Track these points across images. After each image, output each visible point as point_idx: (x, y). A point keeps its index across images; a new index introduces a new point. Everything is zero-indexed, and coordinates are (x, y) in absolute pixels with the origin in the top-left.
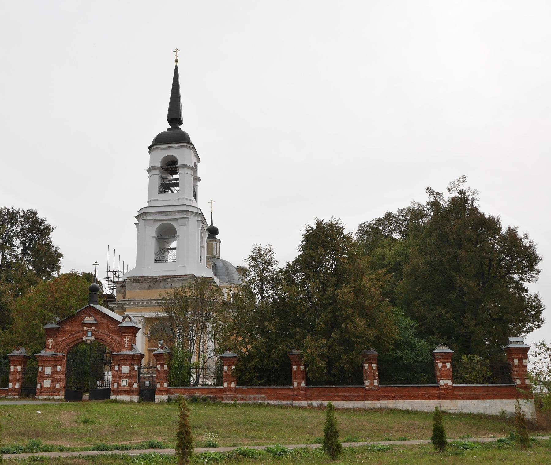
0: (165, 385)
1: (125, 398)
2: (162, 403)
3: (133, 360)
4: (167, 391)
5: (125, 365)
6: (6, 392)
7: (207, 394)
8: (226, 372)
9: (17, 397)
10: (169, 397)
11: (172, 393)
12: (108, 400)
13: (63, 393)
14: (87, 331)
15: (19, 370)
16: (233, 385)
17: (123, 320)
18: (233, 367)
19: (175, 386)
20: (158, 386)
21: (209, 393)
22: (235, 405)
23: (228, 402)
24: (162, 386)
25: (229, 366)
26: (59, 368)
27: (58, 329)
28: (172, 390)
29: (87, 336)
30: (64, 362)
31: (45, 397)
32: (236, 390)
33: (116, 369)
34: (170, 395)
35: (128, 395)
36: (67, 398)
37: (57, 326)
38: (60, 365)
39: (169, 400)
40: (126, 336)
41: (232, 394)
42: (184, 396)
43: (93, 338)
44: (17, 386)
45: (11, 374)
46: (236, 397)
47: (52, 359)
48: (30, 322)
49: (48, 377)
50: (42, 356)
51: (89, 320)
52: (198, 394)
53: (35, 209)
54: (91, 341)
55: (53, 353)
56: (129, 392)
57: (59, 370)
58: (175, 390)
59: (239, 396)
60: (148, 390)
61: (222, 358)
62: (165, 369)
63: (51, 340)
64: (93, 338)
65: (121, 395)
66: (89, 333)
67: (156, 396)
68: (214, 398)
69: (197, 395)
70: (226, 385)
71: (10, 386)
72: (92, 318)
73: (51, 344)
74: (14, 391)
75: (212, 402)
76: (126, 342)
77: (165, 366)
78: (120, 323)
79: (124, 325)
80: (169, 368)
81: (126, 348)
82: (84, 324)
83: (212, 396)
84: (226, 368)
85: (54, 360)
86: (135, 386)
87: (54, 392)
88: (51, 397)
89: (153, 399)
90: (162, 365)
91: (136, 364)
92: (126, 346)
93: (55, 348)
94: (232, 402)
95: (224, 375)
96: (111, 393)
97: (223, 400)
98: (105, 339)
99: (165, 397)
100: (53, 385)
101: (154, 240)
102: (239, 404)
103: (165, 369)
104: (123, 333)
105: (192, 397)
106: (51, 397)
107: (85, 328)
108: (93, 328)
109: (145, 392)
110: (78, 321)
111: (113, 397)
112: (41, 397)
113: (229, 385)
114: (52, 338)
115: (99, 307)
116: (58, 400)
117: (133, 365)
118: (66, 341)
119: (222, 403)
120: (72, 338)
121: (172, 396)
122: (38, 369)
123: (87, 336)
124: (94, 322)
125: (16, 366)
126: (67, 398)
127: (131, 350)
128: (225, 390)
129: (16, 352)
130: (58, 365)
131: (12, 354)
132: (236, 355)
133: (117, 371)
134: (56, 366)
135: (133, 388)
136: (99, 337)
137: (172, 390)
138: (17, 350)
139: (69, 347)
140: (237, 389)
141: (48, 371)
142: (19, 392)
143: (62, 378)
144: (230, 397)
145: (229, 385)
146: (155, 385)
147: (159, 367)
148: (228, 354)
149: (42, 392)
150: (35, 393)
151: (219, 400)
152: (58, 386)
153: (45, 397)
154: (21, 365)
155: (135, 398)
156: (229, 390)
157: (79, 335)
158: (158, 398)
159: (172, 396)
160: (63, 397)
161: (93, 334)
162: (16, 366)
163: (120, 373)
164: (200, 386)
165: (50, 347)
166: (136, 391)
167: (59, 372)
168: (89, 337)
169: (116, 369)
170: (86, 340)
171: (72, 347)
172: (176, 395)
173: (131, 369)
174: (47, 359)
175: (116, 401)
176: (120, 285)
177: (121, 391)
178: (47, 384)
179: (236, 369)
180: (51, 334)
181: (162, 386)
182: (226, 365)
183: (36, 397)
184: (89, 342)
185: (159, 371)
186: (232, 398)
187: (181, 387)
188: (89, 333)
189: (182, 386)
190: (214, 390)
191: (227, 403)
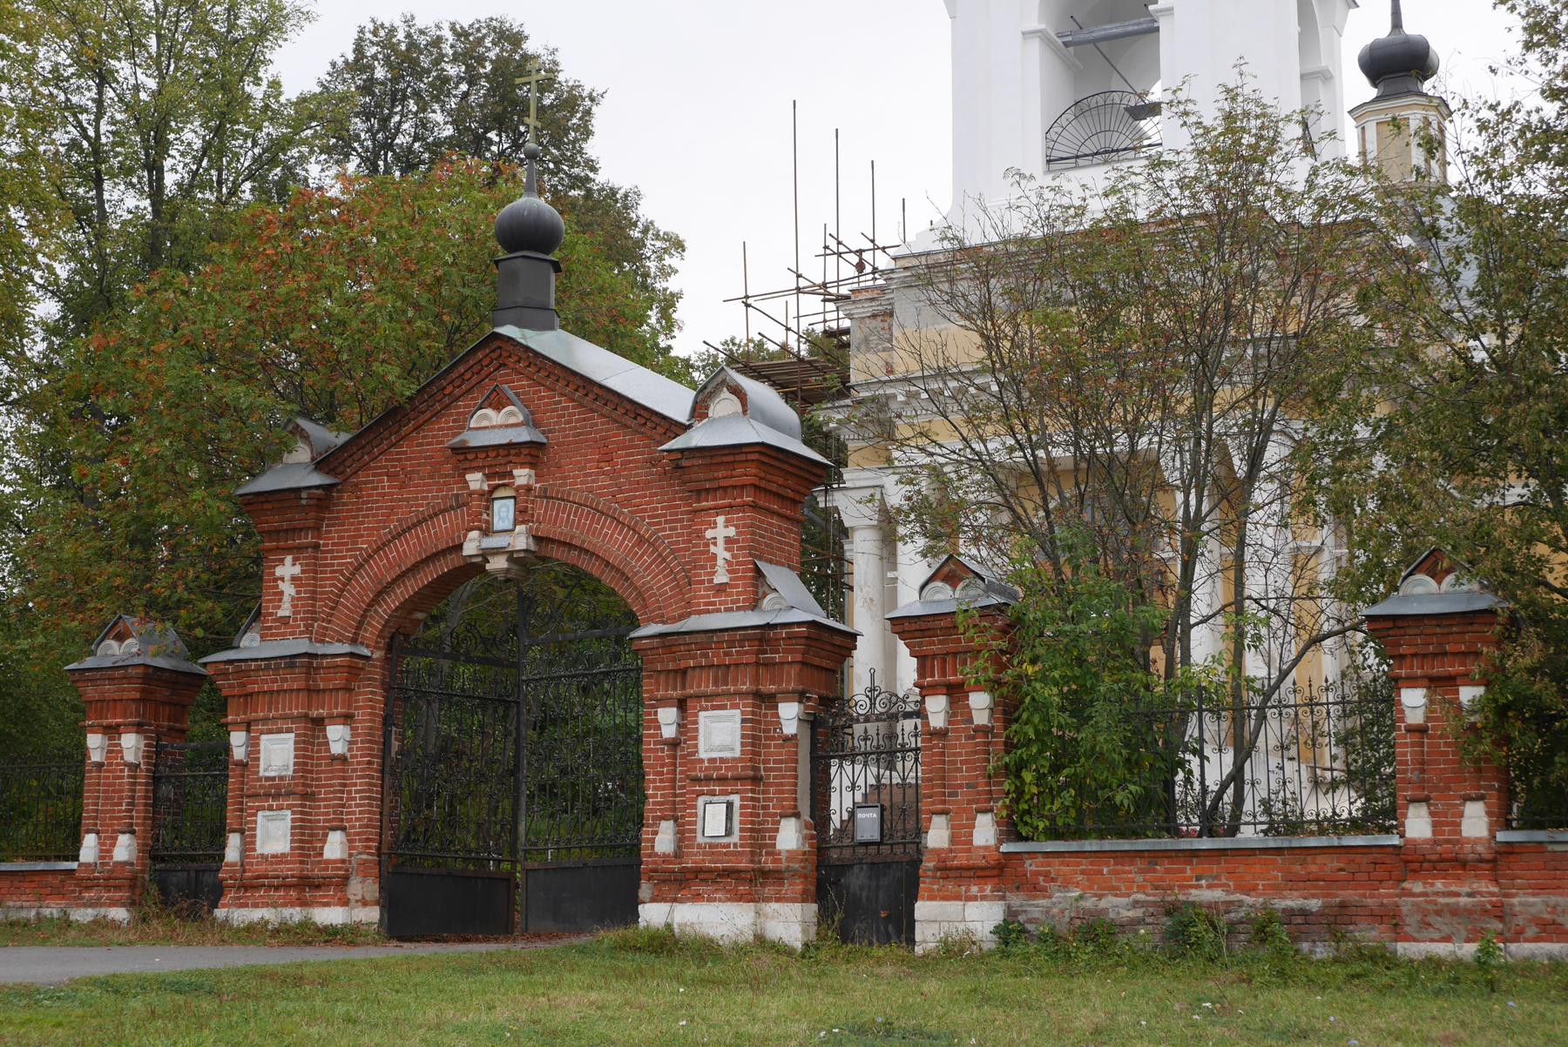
0: (985, 832)
1: (717, 919)
2: (954, 951)
3: (769, 664)
4: (998, 873)
5: (716, 700)
6: (70, 886)
7: (1277, 890)
8: (1420, 730)
9: (120, 914)
10: (1011, 914)
11: (1032, 887)
12: (610, 936)
13: (371, 888)
14: (488, 497)
15: (130, 757)
16: (1475, 822)
17: (699, 410)
18: (1467, 694)
19: (1054, 834)
20: (937, 835)
21: (1294, 882)
22: (1485, 978)
23: (1441, 949)
24: (960, 835)
25: (1442, 684)
26: (337, 737)
27: (324, 499)
28: (1030, 866)
29: (487, 531)
30: (369, 700)
31: (256, 915)
32: (1498, 861)
33: (669, 732)
34: (1016, 900)
35: (739, 898)
36: (408, 917)
37: (317, 479)
38: (347, 719)
39: (1009, 932)
40: (719, 510)
41: (1473, 891)
42: (1118, 906)
43: (521, 541)
44: (124, 849)
45: (91, 777)
46: (1500, 912)
47: (295, 681)
48: (1194, 752)
49: (275, 792)
50: (242, 669)
51: (494, 425)
52: (1217, 895)
53: (515, 18)
54: (511, 556)
55: (300, 646)
56: (748, 877)
57: (337, 748)
58: (1056, 867)
59: (1527, 902)
60: (877, 868)
61: (1386, 630)
62: (981, 718)
63: (288, 569)
64: (520, 541)
65: (697, 898)
66: (503, 512)
67: (922, 909)
68: (1336, 921)
69: (1206, 894)
70: (1418, 825)
71: (89, 847)
72: (513, 413)
73: (288, 589)
74: (108, 880)
75: (1322, 952)
76: (721, 553)
77: (979, 702)
78: (678, 428)
79: (699, 438)
80: (1007, 709)
81: (721, 588)
82: (466, 457)
83: (1314, 904)
84: (1413, 700)
85: (308, 688)
86: (790, 837)
87: (309, 882)
88: (295, 914)
89: (903, 927)
90: (956, 693)
91: (789, 696)
92: (721, 577)
93: (312, 617)
94: (1469, 950)
95: (1406, 751)
96: (645, 890)
97: (1399, 933)
98: (592, 542)
99: (980, 917)
100: (307, 837)
101: (1035, 46)
102: (1526, 968)
103: (981, 718)
104: (700, 493)
105: (1171, 910)
106: (295, 914)
107: (475, 480)
108: (522, 476)
109: (856, 880)
110: (438, 437)
111: (653, 914)
112: (242, 916)
113: (1446, 822)
114: (296, 550)
115: (554, 343)
116: (331, 935)
117: (767, 701)
118: (374, 568)
119: (1389, 961)
120: (408, 549)
121: (1035, 908)
122: (227, 748)
123: (487, 531)
124: (523, 435)
125: (112, 731)
126: (408, 917)
127: (754, 605)
128: (1411, 861)
129: (113, 651)
130: (334, 719)
131: (89, 663)
132: (1485, 601)
133: (674, 744)
134: (319, 723)
135: (773, 853)
136: (559, 531)
137: (1030, 866)
138: (120, 638)
139: (392, 602)
140: (1510, 849)
141: (277, 754)
142: (133, 882)
143: (360, 800)
144: (1455, 911)
145: (1446, 822)
146: (920, 832)
147: (937, 707)
148: (1423, 594)
149: (252, 885)
150: (216, 894)
151: (1368, 935)
152: (334, 847)
153: (256, 915)
154: (139, 728)
155: (789, 922)
156: (1445, 859)
157: (443, 524)
158: (935, 918)
159: (1035, 908)
160: (372, 914)
161: (522, 515)
162: (112, 731)
163: (691, 759)
164: (1248, 835)
165: (285, 611)
166: (795, 873)
167: (342, 759)
168: (504, 532)
169: (669, 732)
170: (486, 554)
171: (409, 606)
172: (1060, 903)
173: (758, 733)
174: (266, 682)
175: (665, 944)
176: (868, 309)
177: (698, 875)
178: (273, 834)
179: (1500, 711)
180: (295, 531)
181: (960, 835)
182: (1412, 682)
183: (220, 913)
184: (498, 564)
185: (941, 734)
186: (1470, 921)
187: (1091, 845)
188: (503, 512)
189: (1102, 836)
190: (1332, 864)
191: (1434, 963)
